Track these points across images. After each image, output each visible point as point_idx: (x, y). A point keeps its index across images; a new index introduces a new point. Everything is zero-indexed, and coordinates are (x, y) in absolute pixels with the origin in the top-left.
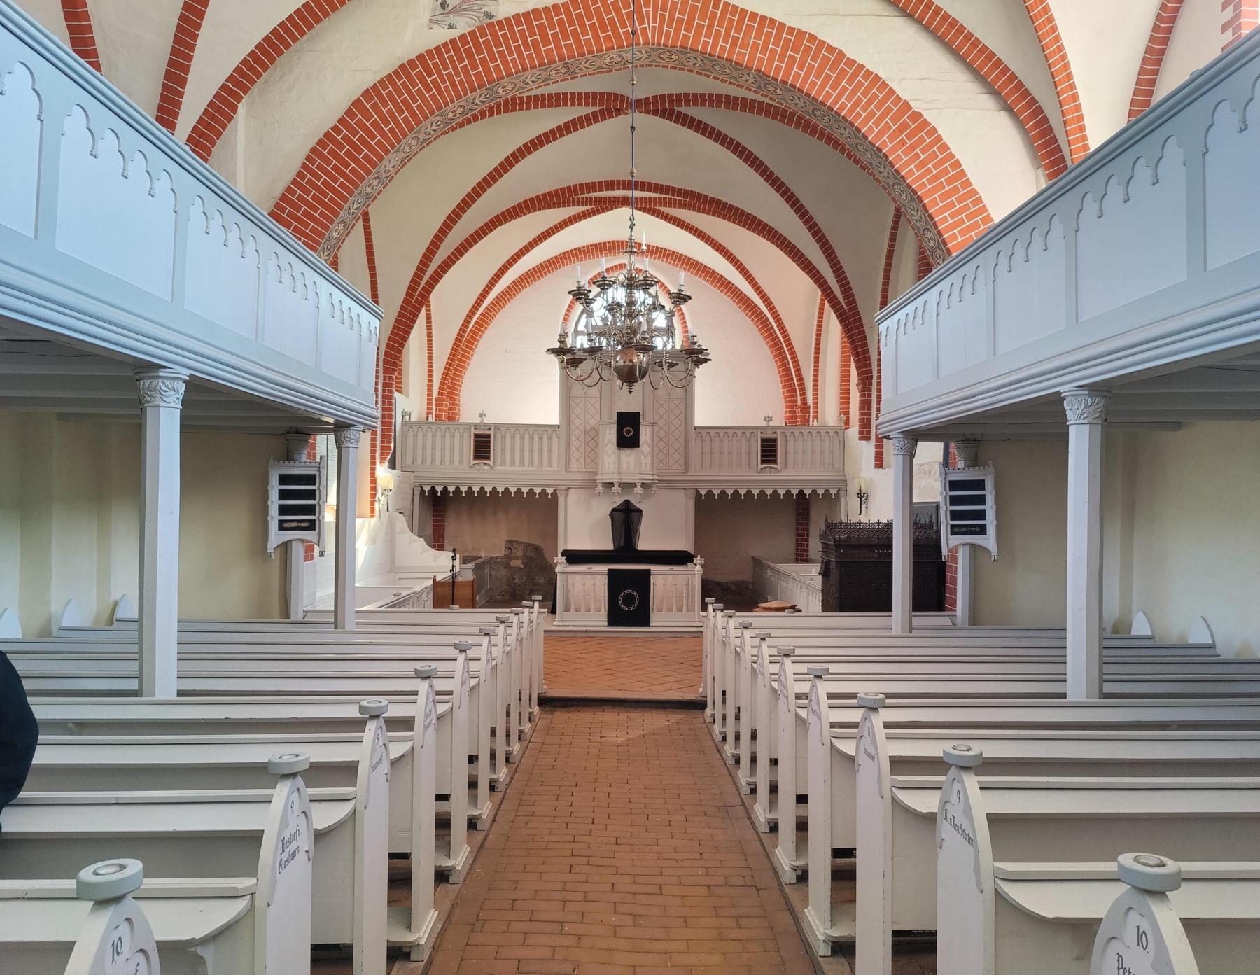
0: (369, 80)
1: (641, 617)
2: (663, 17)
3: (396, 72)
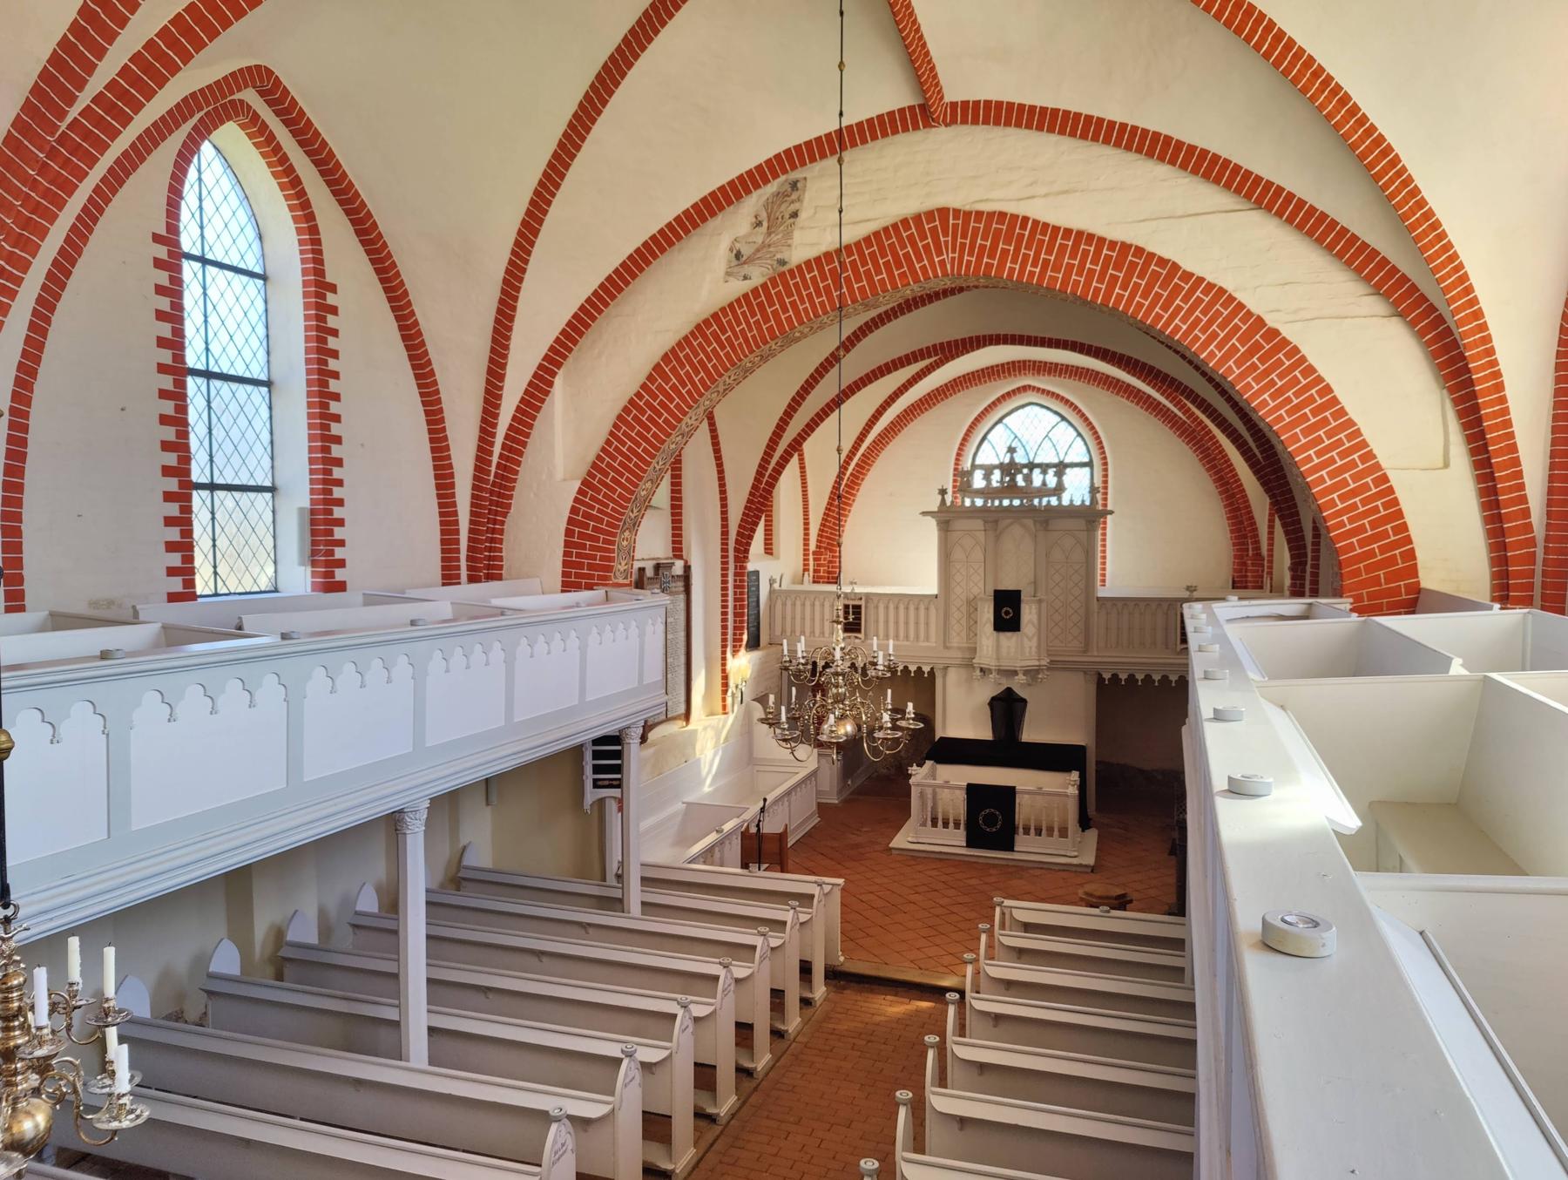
0: (668, 341)
2: (963, 245)
3: (692, 333)
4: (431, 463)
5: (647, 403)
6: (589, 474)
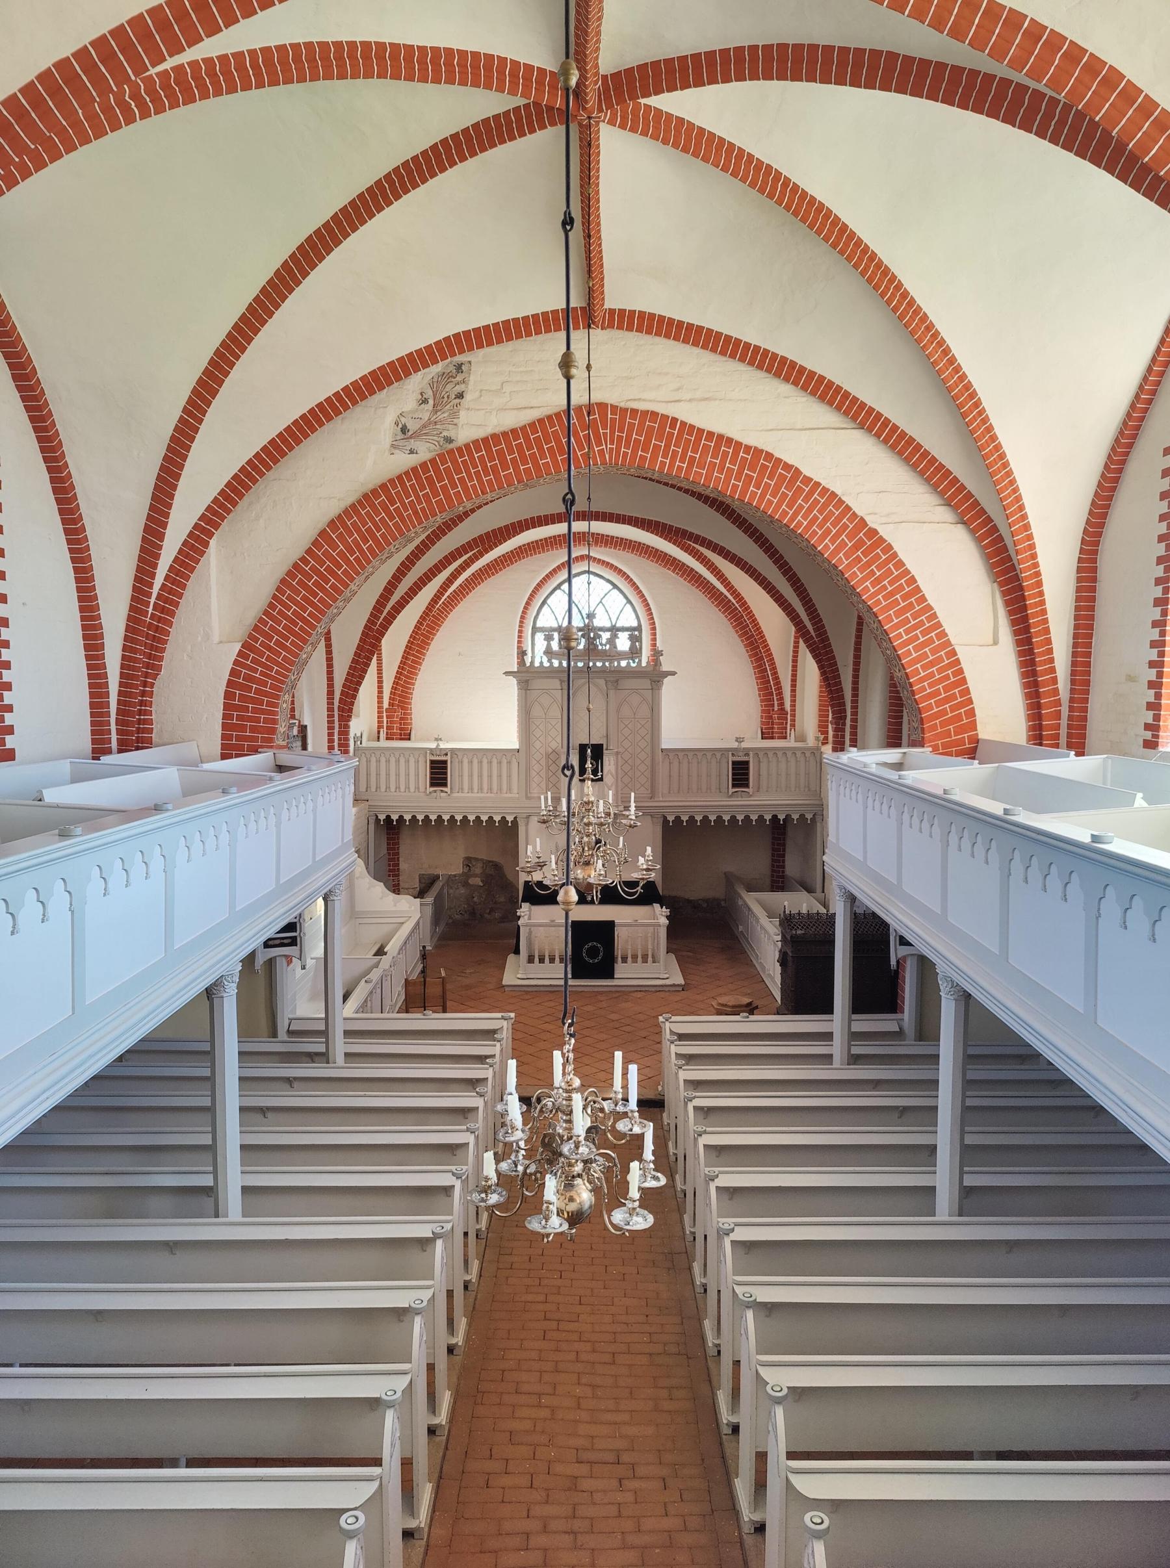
0: (334, 508)
1: (606, 970)
5: (313, 568)
6: (250, 636)
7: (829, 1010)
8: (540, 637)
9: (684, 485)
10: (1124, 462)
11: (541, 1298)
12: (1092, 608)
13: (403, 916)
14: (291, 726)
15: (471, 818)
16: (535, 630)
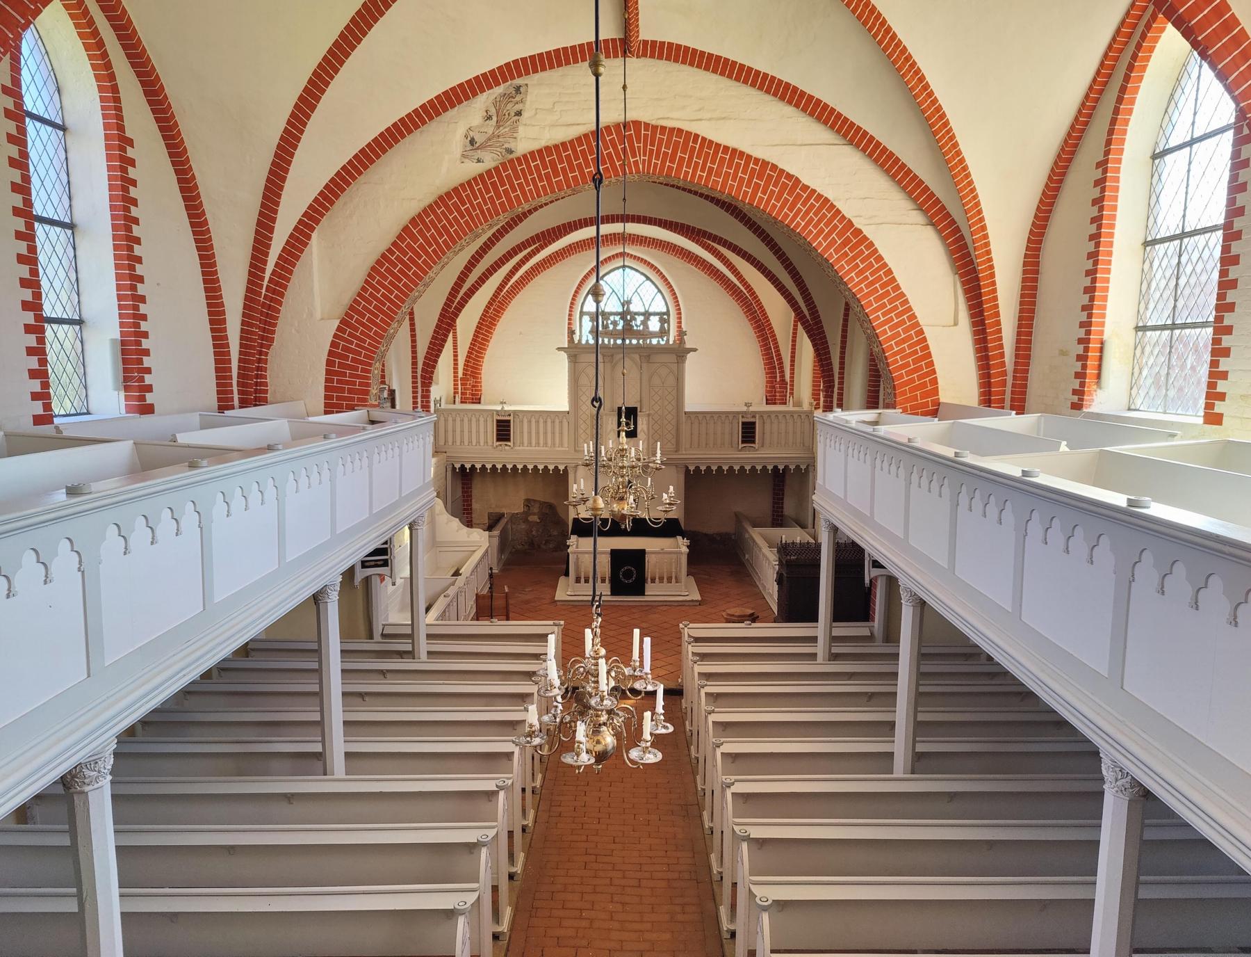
0: (414, 207)
2: (651, 151)
3: (436, 202)
4: (204, 302)
6: (347, 314)
7: (815, 619)
8: (586, 319)
9: (705, 191)
10: (1064, 174)
11: (584, 838)
12: (1034, 296)
13: (475, 545)
14: (382, 390)
15: (530, 467)
16: (582, 314)
